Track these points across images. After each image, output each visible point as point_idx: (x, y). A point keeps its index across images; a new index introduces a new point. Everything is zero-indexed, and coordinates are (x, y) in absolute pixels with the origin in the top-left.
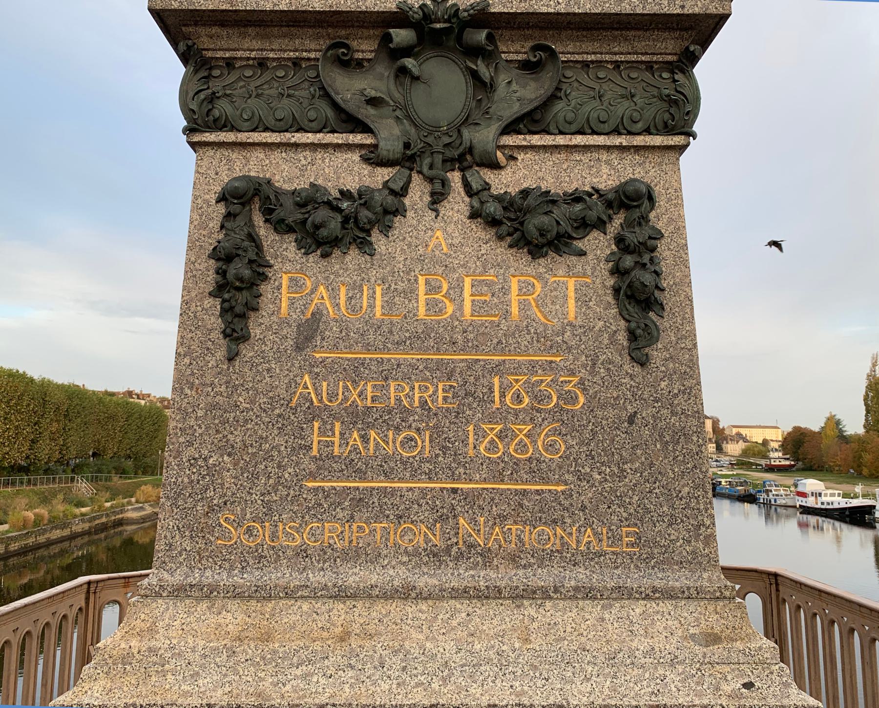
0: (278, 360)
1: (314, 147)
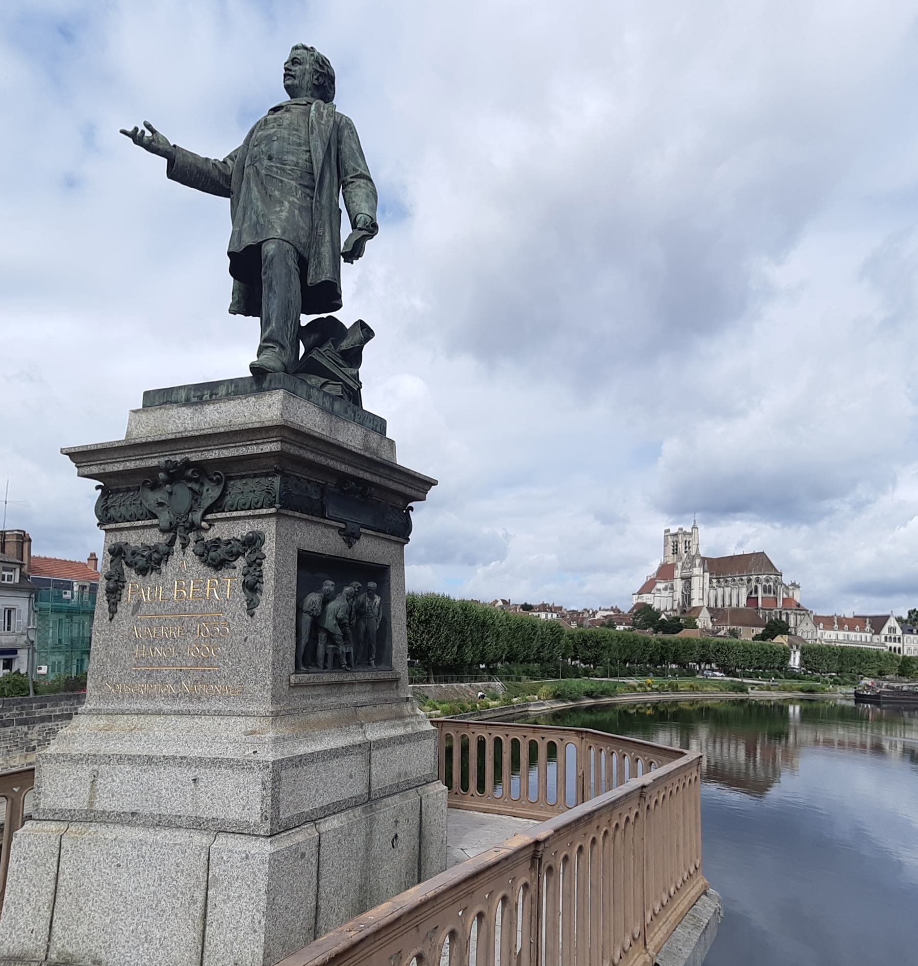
0: (126, 619)
1: (144, 527)
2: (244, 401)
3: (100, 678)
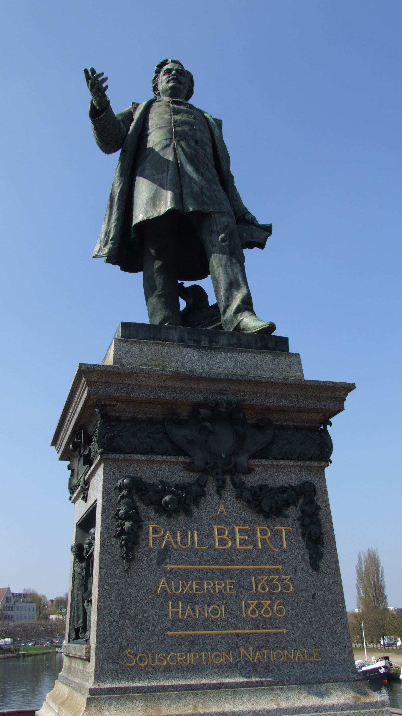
2: (260, 356)
3: (116, 648)
